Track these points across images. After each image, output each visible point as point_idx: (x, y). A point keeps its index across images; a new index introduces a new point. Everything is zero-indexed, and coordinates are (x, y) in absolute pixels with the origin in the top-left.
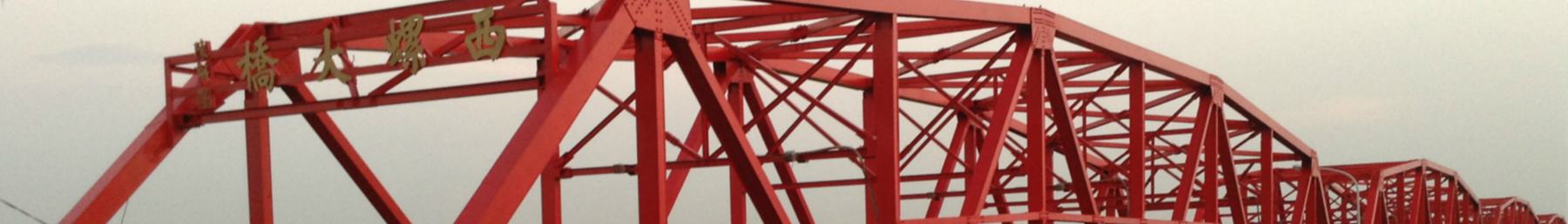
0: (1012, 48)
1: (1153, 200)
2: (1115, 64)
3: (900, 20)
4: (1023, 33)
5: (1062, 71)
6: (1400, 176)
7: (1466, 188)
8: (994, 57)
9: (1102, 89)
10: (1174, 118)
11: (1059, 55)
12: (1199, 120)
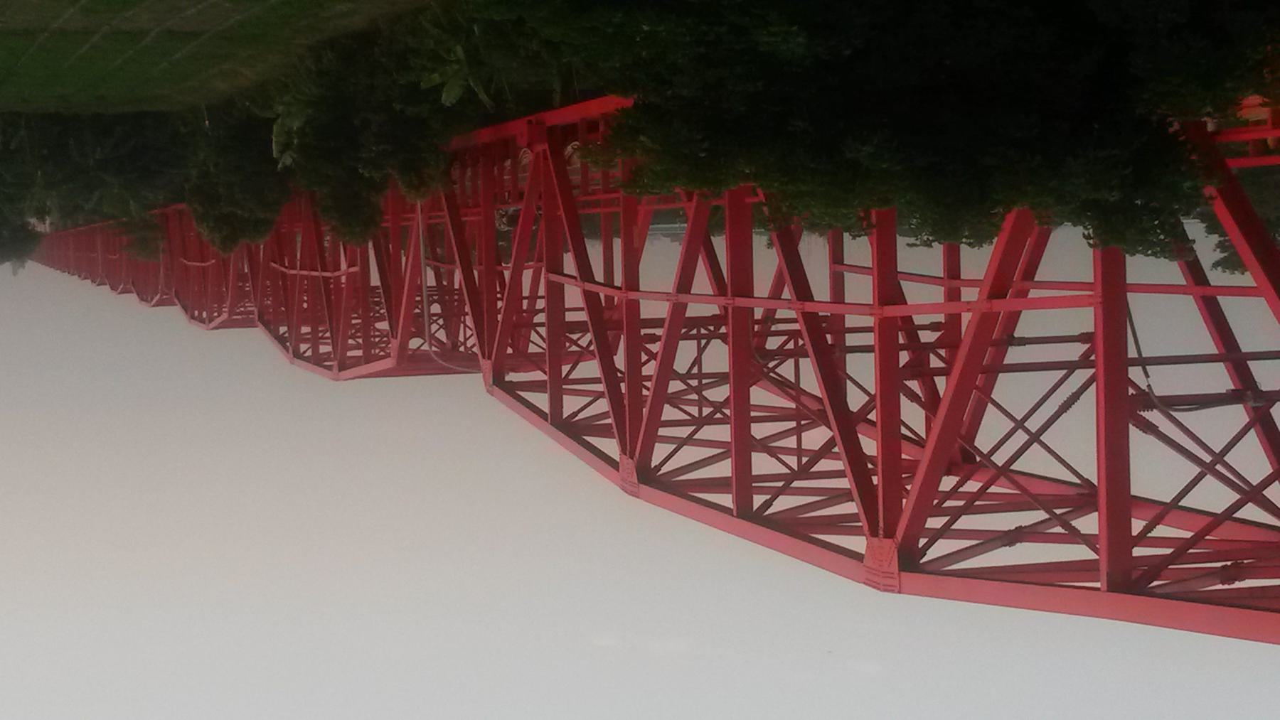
0: (922, 542)
1: (699, 331)
2: (769, 514)
3: (1098, 585)
4: (910, 560)
5: (851, 508)
6: (368, 359)
7: (276, 342)
8: (944, 532)
9: (786, 484)
10: (681, 443)
11: (856, 532)
12: (652, 439)
